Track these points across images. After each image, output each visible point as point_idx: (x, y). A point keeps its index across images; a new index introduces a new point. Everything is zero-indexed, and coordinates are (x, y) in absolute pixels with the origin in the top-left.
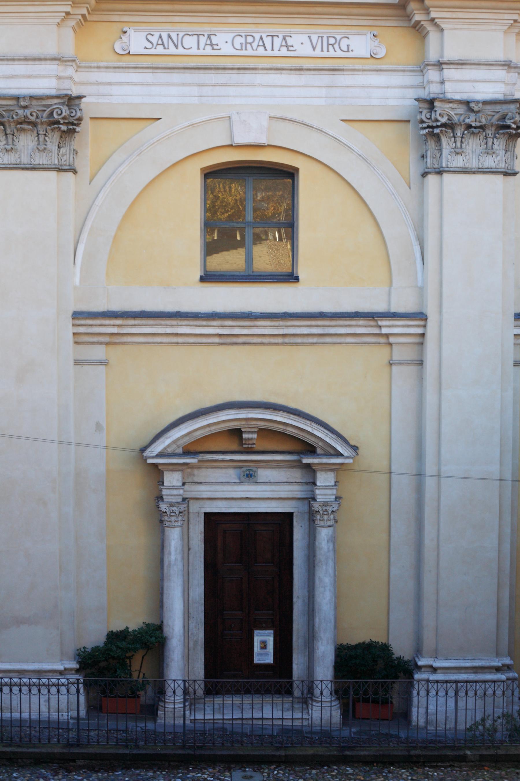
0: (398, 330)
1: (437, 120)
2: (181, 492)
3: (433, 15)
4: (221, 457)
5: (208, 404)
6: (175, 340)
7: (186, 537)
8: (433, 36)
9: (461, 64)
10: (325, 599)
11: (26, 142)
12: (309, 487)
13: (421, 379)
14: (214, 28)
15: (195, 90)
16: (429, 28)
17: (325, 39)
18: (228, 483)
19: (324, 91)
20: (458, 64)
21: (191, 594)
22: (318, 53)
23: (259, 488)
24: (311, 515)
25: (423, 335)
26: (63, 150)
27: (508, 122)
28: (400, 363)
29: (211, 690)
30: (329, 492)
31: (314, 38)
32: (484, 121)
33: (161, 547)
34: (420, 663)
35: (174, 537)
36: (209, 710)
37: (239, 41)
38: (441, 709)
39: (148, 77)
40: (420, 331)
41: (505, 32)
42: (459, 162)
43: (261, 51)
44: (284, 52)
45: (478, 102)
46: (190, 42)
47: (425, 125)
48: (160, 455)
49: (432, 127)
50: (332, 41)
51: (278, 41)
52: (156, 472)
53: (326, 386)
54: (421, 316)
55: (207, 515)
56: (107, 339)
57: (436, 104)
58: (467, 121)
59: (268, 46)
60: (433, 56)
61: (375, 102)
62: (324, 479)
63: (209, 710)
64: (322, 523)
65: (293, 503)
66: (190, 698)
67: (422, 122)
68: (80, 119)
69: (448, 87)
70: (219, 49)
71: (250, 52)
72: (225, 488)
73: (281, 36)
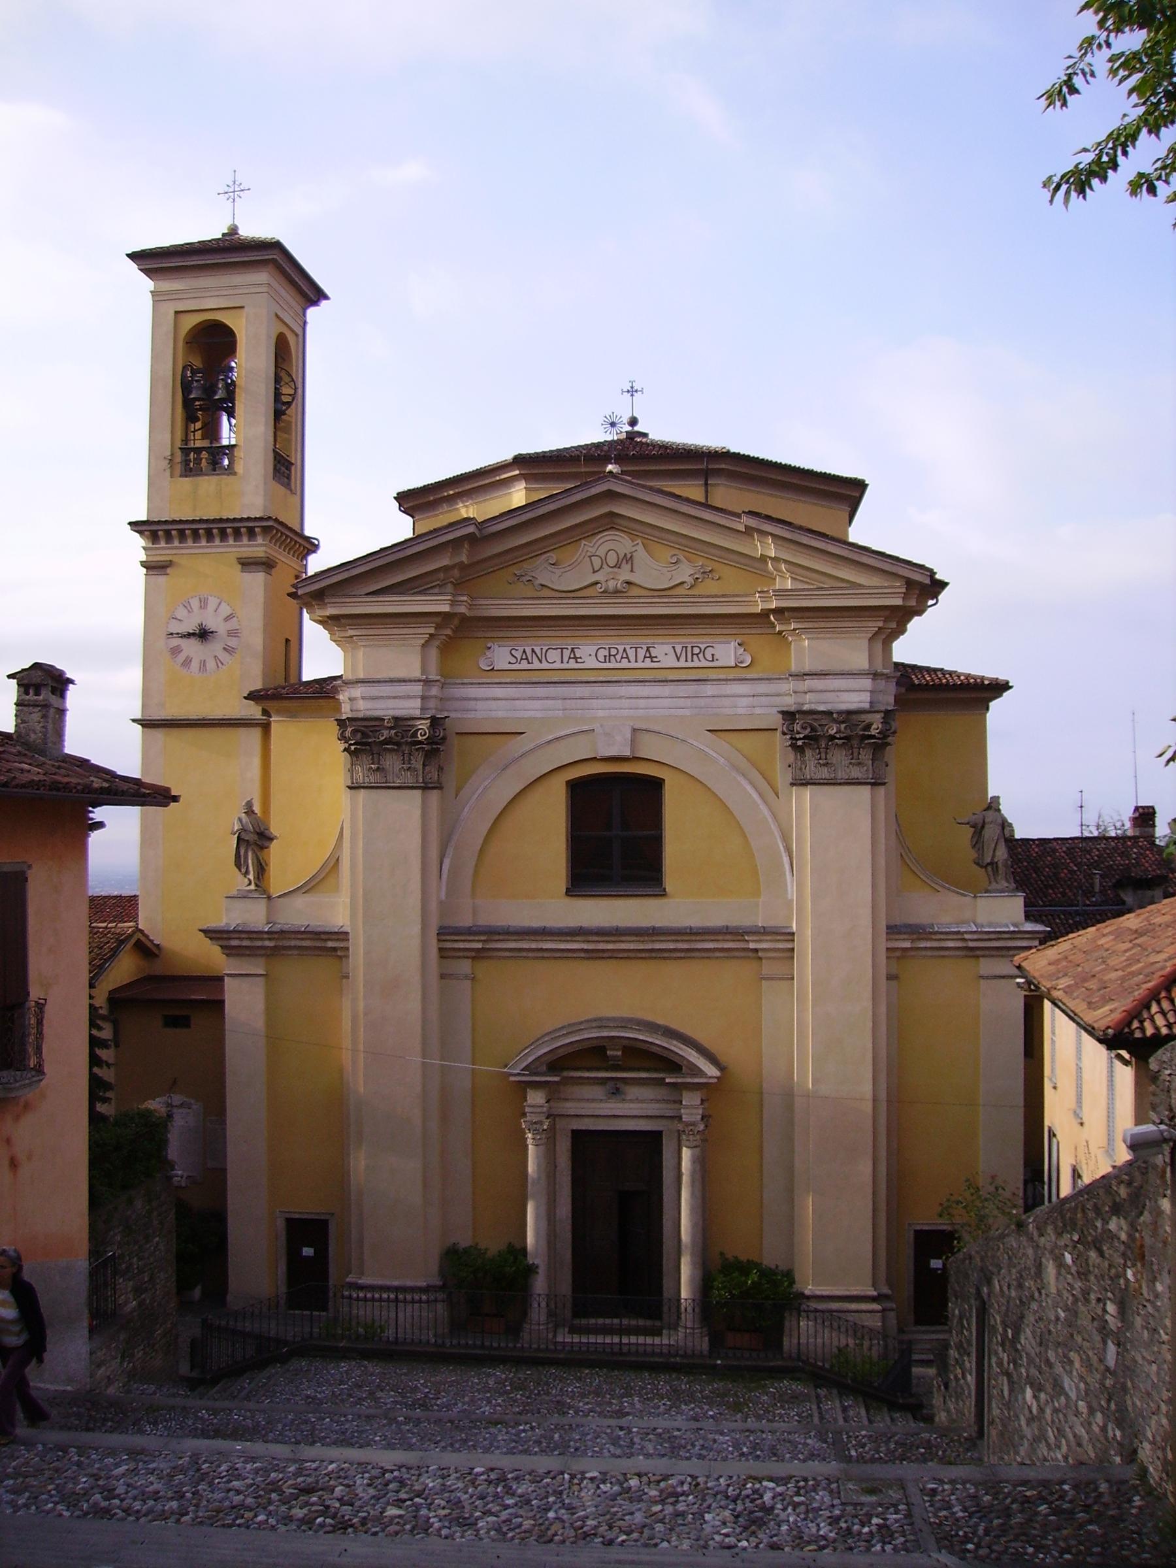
6: (540, 954)
14: (577, 641)
17: (689, 649)
19: (688, 702)
22: (682, 664)
23: (626, 1105)
25: (793, 949)
30: (695, 1111)
31: (679, 648)
37: (602, 653)
38: (827, 1341)
40: (789, 946)
43: (624, 664)
46: (554, 655)
50: (696, 651)
56: (473, 954)
59: (632, 658)
61: (740, 711)
65: (664, 1122)
68: (444, 738)
70: (1088, 82)
72: (593, 1105)
73: (645, 647)
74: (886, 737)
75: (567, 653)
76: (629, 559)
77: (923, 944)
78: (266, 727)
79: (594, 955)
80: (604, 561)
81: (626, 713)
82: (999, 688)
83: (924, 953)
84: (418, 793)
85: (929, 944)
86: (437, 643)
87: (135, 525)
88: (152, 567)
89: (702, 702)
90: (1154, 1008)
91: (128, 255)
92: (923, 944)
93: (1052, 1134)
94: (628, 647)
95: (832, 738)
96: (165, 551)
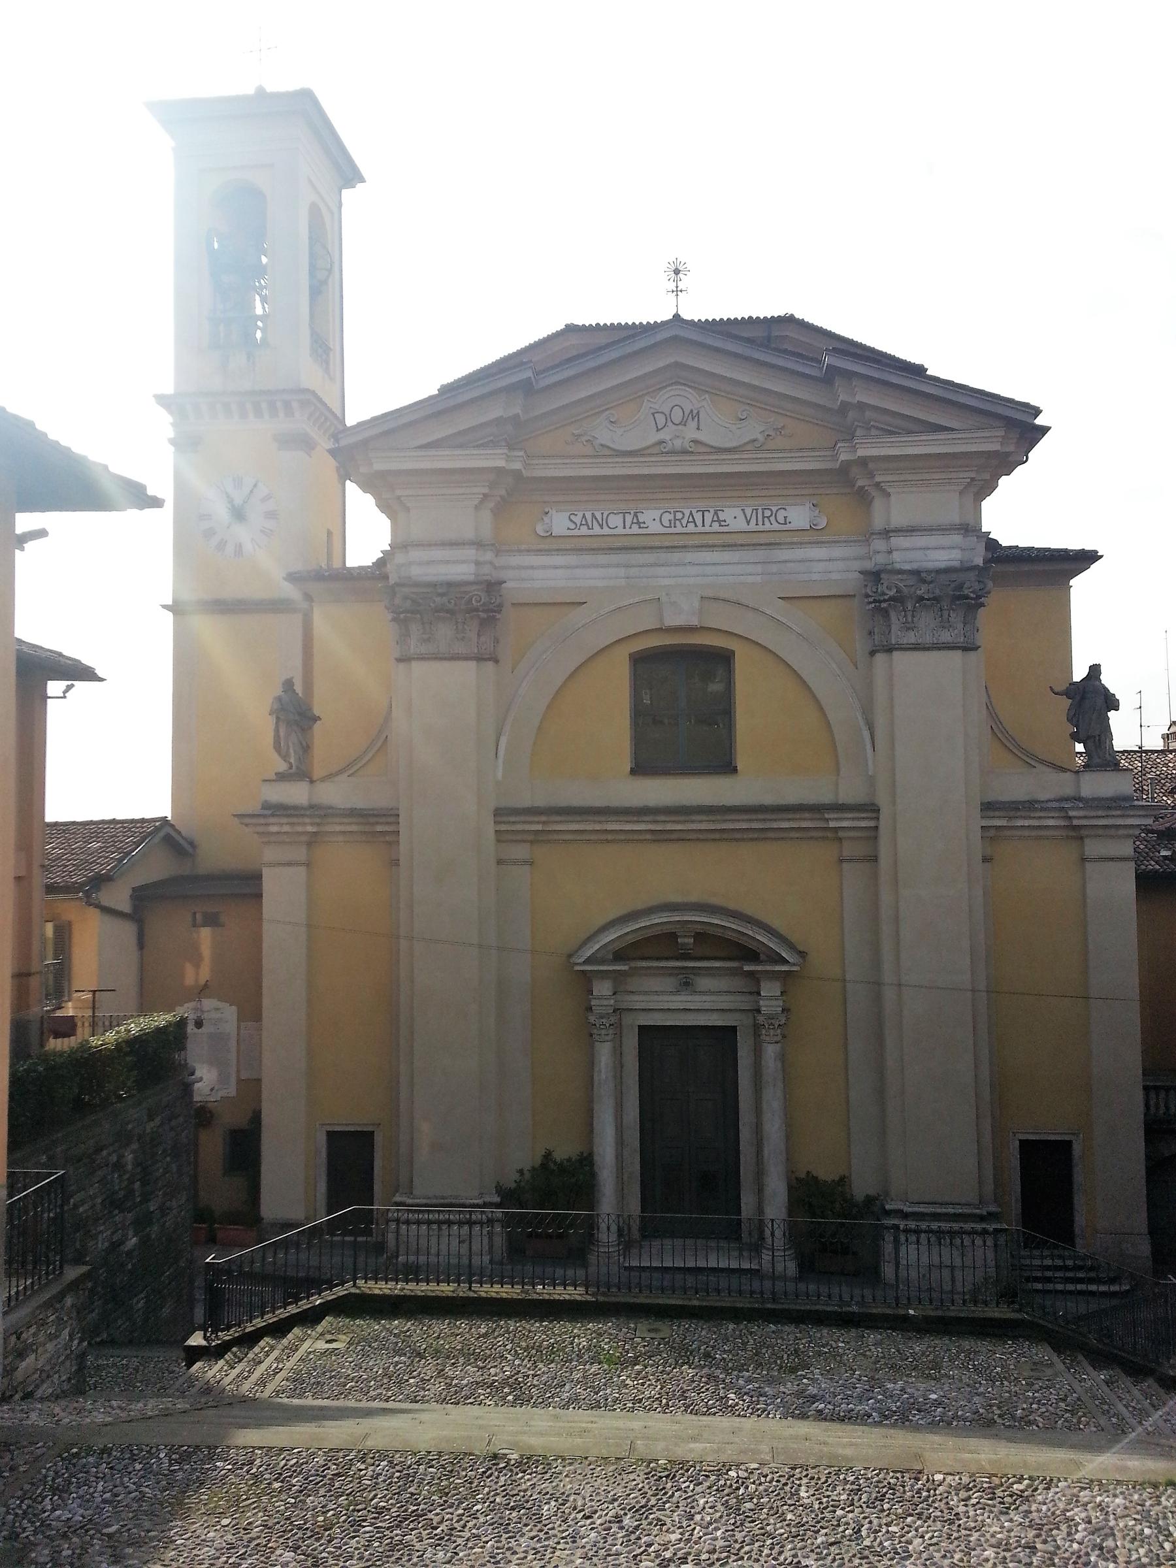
0: (848, 829)
1: (884, 594)
2: (612, 1002)
3: (878, 479)
4: (655, 964)
5: (640, 906)
7: (618, 1053)
8: (878, 504)
9: (911, 530)
10: (773, 1128)
12: (752, 998)
13: (875, 876)
15: (622, 572)
16: (874, 494)
17: (760, 512)
18: (663, 993)
19: (759, 568)
20: (907, 531)
21: (625, 1117)
22: (752, 526)
23: (697, 998)
24: (757, 1028)
25: (876, 828)
26: (483, 639)
27: (966, 592)
30: (774, 1003)
31: (748, 511)
32: (937, 591)
33: (591, 1064)
34: (887, 1207)
35: (604, 1054)
36: (645, 1257)
37: (667, 518)
40: (872, 824)
42: (911, 638)
44: (716, 527)
45: (929, 572)
46: (615, 520)
47: (871, 599)
48: (588, 961)
49: (880, 602)
50: (768, 513)
51: (709, 517)
52: (586, 979)
54: (872, 809)
55: (642, 1029)
56: (531, 837)
57: (883, 576)
58: (918, 592)
59: (699, 523)
60: (878, 522)
61: (815, 577)
62: (770, 989)
63: (645, 1257)
64: (768, 1039)
65: (737, 1016)
66: (626, 1244)
67: (867, 596)
68: (500, 606)
71: (679, 529)
73: (712, 511)
74: (979, 597)
75: (629, 518)
76: (695, 415)
77: (1020, 823)
79: (662, 837)
80: (668, 418)
81: (692, 581)
82: (1085, 559)
83: (1019, 833)
84: (472, 664)
85: (1026, 823)
86: (491, 505)
87: (162, 400)
89: (774, 568)
92: (1020, 823)
94: (694, 511)
95: (921, 599)
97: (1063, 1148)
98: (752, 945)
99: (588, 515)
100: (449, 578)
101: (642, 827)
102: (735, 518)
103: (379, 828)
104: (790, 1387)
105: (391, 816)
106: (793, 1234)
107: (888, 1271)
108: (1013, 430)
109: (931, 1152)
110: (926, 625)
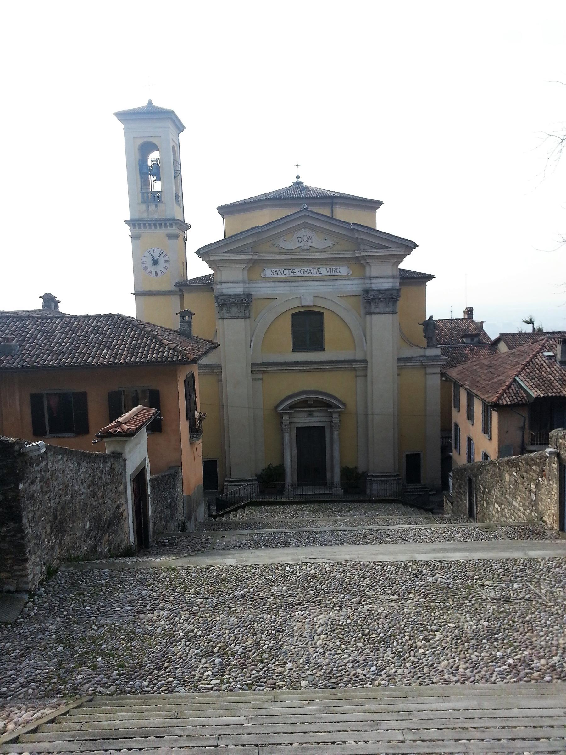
0: (358, 367)
7: (290, 435)
8: (367, 268)
9: (377, 278)
10: (336, 454)
11: (234, 310)
15: (288, 288)
19: (331, 287)
22: (329, 274)
24: (331, 427)
28: (359, 376)
29: (300, 485)
31: (328, 269)
33: (283, 438)
35: (287, 436)
37: (302, 271)
39: (273, 284)
40: (365, 366)
41: (393, 265)
42: (377, 310)
43: (310, 274)
45: (383, 290)
46: (286, 272)
48: (281, 410)
51: (315, 271)
52: (281, 416)
53: (333, 385)
54: (365, 361)
60: (368, 274)
61: (349, 290)
62: (335, 416)
69: (373, 285)
71: (306, 275)
75: (290, 271)
77: (408, 364)
78: (181, 296)
80: (302, 239)
82: (431, 277)
86: (247, 269)
87: (126, 222)
88: (134, 237)
90: (505, 395)
91: (380, 203)
92: (408, 364)
93: (456, 426)
95: (380, 299)
96: (138, 231)
97: (418, 455)
98: (331, 403)
99: (278, 270)
100: (235, 293)
101: (296, 368)
102: (324, 271)
103: (215, 371)
104: (349, 514)
105: (219, 367)
106: (342, 484)
107: (368, 492)
108: (408, 246)
109: (381, 458)
110: (382, 307)
